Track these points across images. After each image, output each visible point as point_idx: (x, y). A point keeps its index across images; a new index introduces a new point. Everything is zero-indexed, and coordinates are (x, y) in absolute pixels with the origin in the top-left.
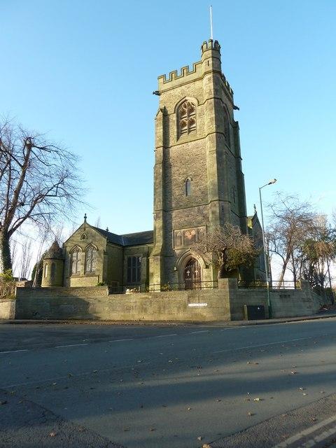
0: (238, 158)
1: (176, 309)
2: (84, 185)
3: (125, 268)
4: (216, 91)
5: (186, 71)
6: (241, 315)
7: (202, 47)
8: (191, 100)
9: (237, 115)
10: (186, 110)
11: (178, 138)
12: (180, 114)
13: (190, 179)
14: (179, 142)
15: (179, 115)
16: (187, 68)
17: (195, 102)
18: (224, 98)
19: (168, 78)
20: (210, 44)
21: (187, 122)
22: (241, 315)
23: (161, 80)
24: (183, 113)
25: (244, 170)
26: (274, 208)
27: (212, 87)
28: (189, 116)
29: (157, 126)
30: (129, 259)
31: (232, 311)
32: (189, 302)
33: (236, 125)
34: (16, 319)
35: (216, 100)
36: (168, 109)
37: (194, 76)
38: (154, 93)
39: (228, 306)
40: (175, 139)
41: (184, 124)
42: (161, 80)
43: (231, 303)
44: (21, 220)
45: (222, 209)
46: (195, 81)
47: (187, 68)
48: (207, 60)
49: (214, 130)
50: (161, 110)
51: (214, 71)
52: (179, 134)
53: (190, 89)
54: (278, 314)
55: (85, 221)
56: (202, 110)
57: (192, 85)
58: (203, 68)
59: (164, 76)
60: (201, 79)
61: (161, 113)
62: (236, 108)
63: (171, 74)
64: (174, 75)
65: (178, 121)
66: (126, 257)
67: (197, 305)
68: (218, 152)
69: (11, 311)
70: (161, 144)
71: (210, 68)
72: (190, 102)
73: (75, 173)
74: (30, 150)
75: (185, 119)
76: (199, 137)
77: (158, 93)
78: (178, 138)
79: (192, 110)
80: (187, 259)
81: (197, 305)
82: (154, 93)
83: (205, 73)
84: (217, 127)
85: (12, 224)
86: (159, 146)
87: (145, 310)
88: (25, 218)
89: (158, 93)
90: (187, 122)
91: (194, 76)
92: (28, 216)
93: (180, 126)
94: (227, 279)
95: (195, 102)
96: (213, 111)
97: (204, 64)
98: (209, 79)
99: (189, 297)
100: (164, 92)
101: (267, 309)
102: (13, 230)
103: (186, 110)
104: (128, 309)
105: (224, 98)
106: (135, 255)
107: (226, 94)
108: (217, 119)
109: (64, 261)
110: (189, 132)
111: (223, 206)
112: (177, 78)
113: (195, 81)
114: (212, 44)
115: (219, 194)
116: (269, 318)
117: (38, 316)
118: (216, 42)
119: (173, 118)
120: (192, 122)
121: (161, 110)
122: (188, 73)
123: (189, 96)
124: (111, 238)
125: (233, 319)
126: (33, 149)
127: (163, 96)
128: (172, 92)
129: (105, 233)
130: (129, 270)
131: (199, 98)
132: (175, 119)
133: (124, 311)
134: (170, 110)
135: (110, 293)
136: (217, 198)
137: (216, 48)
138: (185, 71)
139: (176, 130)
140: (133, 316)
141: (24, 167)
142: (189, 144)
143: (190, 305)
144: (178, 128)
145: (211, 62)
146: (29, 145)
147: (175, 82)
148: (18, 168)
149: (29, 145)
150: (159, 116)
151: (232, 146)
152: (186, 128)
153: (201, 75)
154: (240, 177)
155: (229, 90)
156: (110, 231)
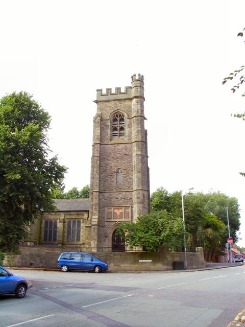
25: (149, 166)
30: (46, 222)
57: (123, 103)
60: (131, 99)
61: (99, 118)
66: (43, 221)
90: (118, 128)
118: (143, 76)
130: (46, 232)
142: (120, 145)
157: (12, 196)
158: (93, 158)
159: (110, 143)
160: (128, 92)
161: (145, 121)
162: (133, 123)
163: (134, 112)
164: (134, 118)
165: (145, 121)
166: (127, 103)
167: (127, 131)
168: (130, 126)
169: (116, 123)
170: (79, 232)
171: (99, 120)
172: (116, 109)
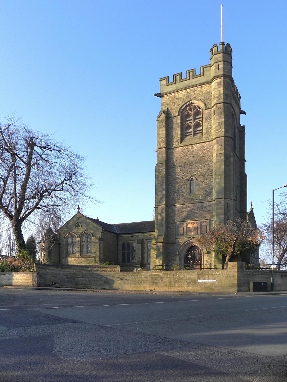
0: (243, 161)
1: (186, 283)
2: (88, 182)
3: (119, 252)
4: (226, 95)
5: (191, 74)
6: (246, 288)
7: (212, 50)
8: (196, 103)
9: (243, 120)
10: (192, 113)
11: (182, 140)
12: (184, 116)
13: (194, 178)
14: (183, 144)
15: (184, 118)
16: (194, 70)
17: (202, 105)
18: (233, 103)
19: (171, 80)
20: (220, 48)
21: (192, 125)
22: (246, 288)
23: (164, 82)
24: (188, 115)
25: (247, 172)
26: (279, 207)
27: (222, 92)
28: (194, 119)
29: (158, 127)
30: (123, 245)
31: (239, 285)
32: (199, 278)
33: (242, 130)
34: (38, 286)
35: (226, 105)
36: (172, 111)
37: (202, 79)
38: (155, 95)
39: (236, 282)
40: (179, 141)
41: (189, 127)
42: (164, 82)
43: (239, 280)
44: (29, 211)
45: (227, 206)
46: (202, 84)
47: (194, 70)
48: (217, 64)
49: (223, 134)
50: (164, 112)
51: (225, 76)
52: (183, 136)
53: (196, 92)
54: (277, 288)
55: (79, 212)
56: (210, 114)
57: (199, 89)
58: (212, 72)
59: (167, 78)
60: (209, 82)
61: (163, 116)
62: (243, 112)
63: (175, 76)
64: (178, 77)
65: (182, 123)
66: (120, 243)
67: (207, 281)
68: (225, 155)
69: (33, 281)
70: (164, 145)
71: (221, 73)
72: (196, 105)
73: (81, 171)
74: (32, 149)
75: (190, 122)
76: (204, 139)
77: (160, 95)
78: (182, 140)
79: (198, 113)
80: (189, 246)
81: (207, 281)
82: (155, 95)
83: (215, 77)
84: (226, 131)
85: (21, 215)
86: (161, 146)
87: (156, 284)
88: (33, 209)
89: (160, 95)
90: (192, 125)
91: (202, 79)
92: (36, 207)
93: (184, 128)
94: (236, 263)
95: (202, 105)
96: (222, 116)
97: (213, 68)
98: (219, 84)
99: (199, 275)
100: (166, 94)
101: (269, 284)
102: (23, 219)
103: (192, 113)
104: (140, 283)
105: (233, 103)
106: (129, 242)
107: (235, 99)
108: (226, 124)
109: (59, 244)
110: (195, 134)
111: (228, 204)
112: (181, 81)
113: (202, 84)
114: (223, 47)
115: (225, 193)
116: (271, 291)
117: (56, 285)
118: (228, 45)
119: (178, 120)
120: (198, 125)
121: (164, 112)
122: (195, 76)
123: (195, 99)
124: (106, 228)
125: (239, 291)
126: (35, 148)
127: (165, 99)
128: (176, 94)
129: (97, 221)
130: (123, 254)
131: (207, 102)
132: (179, 121)
133: (135, 284)
134: (174, 112)
135: (121, 271)
136: (223, 196)
137: (227, 51)
138: (191, 74)
139: (179, 132)
140: (144, 287)
141: (29, 165)
142: (195, 146)
143: (199, 281)
144: (182, 130)
145: (221, 66)
146: (31, 144)
147: (179, 85)
148: (23, 165)
149: (31, 144)
150: (161, 119)
151: (237, 150)
152: (191, 130)
153: (209, 79)
154: (243, 178)
155: (237, 95)
156: (101, 220)
157: (24, 217)
158: (157, 167)
159: (180, 145)
160: (205, 73)
161: (242, 116)
162: (213, 115)
163: (214, 99)
164: (215, 107)
165: (242, 116)
166: (205, 88)
167: (205, 126)
168: (209, 118)
169: (190, 118)
170: (10, 294)
171: (164, 118)
172: (189, 99)
